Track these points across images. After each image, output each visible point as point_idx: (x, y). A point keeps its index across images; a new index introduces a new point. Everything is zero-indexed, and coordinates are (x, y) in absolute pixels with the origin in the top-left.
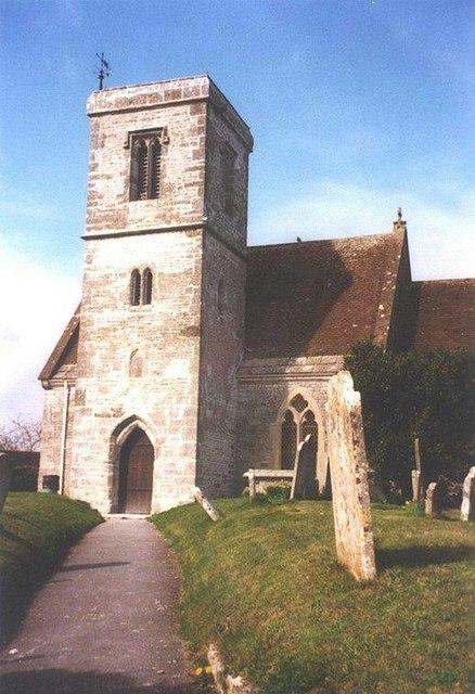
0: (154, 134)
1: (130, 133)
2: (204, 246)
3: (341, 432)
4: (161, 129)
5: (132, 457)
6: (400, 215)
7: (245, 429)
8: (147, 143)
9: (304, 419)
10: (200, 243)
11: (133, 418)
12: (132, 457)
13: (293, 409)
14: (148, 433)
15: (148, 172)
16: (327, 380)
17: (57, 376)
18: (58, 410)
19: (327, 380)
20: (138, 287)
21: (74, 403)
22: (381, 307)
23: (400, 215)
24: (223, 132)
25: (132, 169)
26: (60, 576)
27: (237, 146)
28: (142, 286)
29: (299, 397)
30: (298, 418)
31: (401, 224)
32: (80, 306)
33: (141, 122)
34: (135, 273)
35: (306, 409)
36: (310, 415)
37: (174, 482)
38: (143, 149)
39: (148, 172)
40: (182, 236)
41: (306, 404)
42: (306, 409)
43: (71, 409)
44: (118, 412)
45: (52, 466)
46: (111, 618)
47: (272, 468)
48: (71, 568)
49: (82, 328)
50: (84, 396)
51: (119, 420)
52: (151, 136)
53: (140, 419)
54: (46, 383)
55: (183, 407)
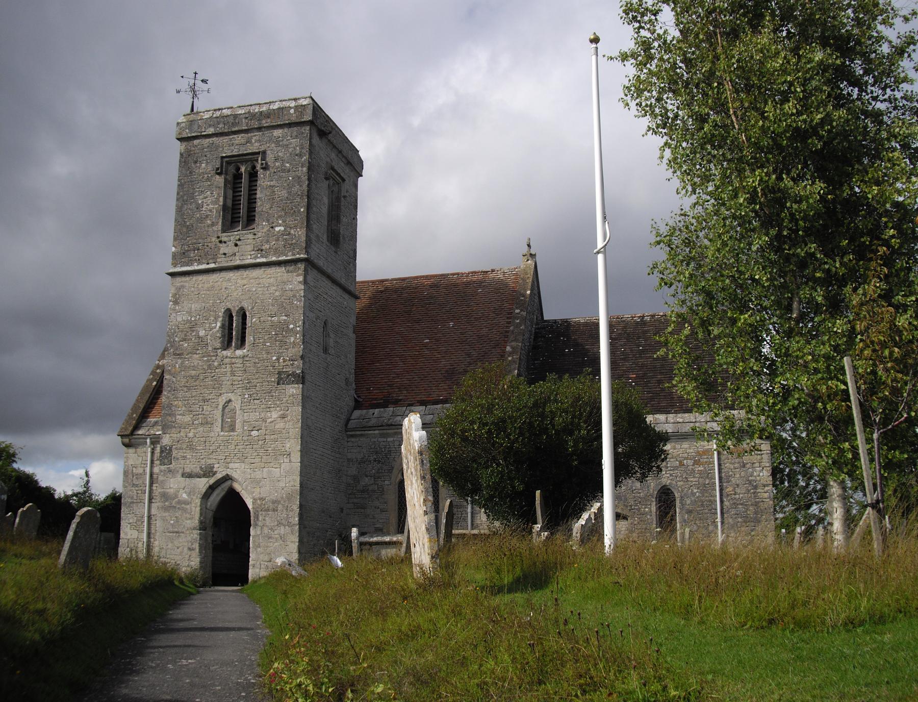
0: (250, 158)
1: (222, 157)
2: (305, 282)
3: (413, 470)
4: (258, 153)
5: (228, 520)
6: (529, 246)
7: (347, 499)
8: (243, 169)
10: (301, 278)
11: (227, 478)
12: (228, 520)
15: (243, 201)
17: (140, 432)
18: (140, 471)
19: (206, 496)
20: (231, 324)
21: (158, 462)
22: (508, 349)
23: (529, 246)
24: (325, 155)
25: (225, 198)
26: (164, 639)
27: (340, 166)
28: (235, 328)
32: (164, 351)
33: (233, 146)
34: (229, 314)
37: (273, 548)
38: (238, 176)
39: (243, 201)
40: (280, 271)
43: (156, 470)
44: (208, 472)
45: (135, 534)
46: (744, 15)
47: (388, 534)
48: (154, 647)
49: (167, 376)
51: (212, 481)
52: (246, 161)
54: (126, 440)
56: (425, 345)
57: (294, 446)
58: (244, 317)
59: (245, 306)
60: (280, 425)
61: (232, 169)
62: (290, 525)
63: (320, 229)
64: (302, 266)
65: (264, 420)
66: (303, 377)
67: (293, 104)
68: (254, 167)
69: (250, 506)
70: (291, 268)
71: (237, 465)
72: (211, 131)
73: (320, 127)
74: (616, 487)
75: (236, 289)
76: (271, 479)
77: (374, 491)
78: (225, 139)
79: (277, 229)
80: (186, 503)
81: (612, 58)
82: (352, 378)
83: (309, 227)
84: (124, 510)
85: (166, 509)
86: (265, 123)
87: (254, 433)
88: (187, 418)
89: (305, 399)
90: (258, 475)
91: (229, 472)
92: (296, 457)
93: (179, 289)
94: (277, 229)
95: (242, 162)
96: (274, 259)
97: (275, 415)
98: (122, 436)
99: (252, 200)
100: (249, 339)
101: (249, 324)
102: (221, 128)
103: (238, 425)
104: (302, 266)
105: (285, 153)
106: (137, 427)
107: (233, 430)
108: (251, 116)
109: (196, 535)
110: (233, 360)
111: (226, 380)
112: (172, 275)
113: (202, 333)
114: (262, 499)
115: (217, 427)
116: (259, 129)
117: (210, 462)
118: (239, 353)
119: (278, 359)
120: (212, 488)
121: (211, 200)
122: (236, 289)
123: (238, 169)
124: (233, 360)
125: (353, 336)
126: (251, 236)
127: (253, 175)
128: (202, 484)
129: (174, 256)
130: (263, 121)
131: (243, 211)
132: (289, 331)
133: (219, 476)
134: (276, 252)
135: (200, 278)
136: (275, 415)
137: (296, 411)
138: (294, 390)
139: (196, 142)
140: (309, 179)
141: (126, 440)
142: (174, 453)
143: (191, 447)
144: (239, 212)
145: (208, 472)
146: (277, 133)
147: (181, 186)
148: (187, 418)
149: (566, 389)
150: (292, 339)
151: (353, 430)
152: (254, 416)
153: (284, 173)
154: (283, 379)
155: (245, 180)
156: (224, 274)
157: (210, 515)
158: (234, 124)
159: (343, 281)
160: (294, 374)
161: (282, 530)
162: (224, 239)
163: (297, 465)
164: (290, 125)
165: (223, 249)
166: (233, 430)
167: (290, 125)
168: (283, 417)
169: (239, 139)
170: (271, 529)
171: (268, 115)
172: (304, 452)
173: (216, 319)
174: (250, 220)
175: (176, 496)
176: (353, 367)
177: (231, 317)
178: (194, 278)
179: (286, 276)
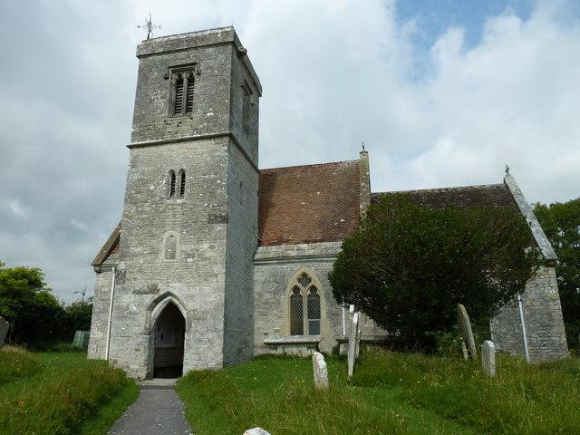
0: (190, 67)
2: (229, 151)
9: (309, 293)
13: (300, 285)
14: (181, 308)
16: (151, 308)
18: (107, 290)
19: (151, 308)
20: (173, 185)
25: (171, 95)
28: (177, 183)
29: (304, 275)
30: (305, 292)
31: (364, 153)
33: (182, 59)
35: (311, 284)
36: (313, 289)
41: (310, 280)
42: (311, 284)
44: (154, 290)
50: (430, 347)
51: (156, 297)
53: (175, 296)
54: (98, 268)
55: (132, 344)
56: (303, 206)
57: (220, 269)
58: (183, 176)
59: (184, 168)
61: (175, 77)
62: (216, 330)
63: (238, 117)
64: (227, 139)
66: (227, 218)
67: (220, 31)
68: (191, 75)
69: (185, 317)
70: (218, 141)
71: (176, 284)
73: (232, 45)
75: (176, 156)
76: (201, 298)
77: (273, 303)
78: (172, 56)
80: (135, 313)
81: (507, 171)
82: (256, 226)
83: (231, 113)
84: (94, 317)
85: (120, 318)
87: (190, 260)
88: (139, 250)
89: (229, 234)
90: (193, 291)
92: (222, 278)
93: (135, 157)
95: (183, 71)
97: (206, 246)
98: (95, 266)
99: (190, 98)
100: (187, 191)
101: (187, 180)
103: (178, 254)
104: (227, 139)
105: (214, 64)
106: (104, 260)
108: (189, 40)
109: (144, 339)
111: (169, 221)
112: (130, 147)
113: (152, 187)
114: (194, 310)
115: (162, 256)
116: (196, 48)
117: (155, 282)
118: (179, 201)
120: (156, 302)
122: (176, 156)
123: (180, 76)
125: (257, 197)
126: (189, 120)
127: (191, 81)
128: (149, 299)
129: (133, 134)
130: (196, 43)
131: (184, 103)
133: (162, 293)
136: (206, 246)
137: (222, 245)
139: (151, 58)
140: (232, 80)
141: (98, 268)
142: (127, 276)
143: (140, 271)
144: (181, 105)
145: (154, 290)
146: (210, 50)
147: (139, 87)
148: (139, 250)
151: (258, 260)
153: (199, 80)
154: (215, 219)
155: (185, 81)
156: (169, 146)
157: (153, 322)
159: (249, 154)
160: (221, 217)
161: (210, 335)
162: (170, 122)
163: (222, 284)
164: (217, 45)
167: (217, 45)
169: (182, 54)
170: (202, 334)
171: (202, 39)
172: (228, 274)
174: (189, 108)
175: (128, 308)
176: (257, 218)
177: (174, 176)
178: (147, 149)
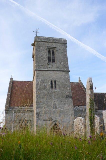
33: (50, 45)
52: (52, 49)
58: (55, 82)
60: (68, 108)
65: (64, 107)
72: (44, 41)
74: (10, 106)
79: (62, 64)
86: (56, 42)
91: (56, 119)
94: (62, 64)
95: (51, 49)
96: (62, 70)
97: (67, 105)
102: (46, 41)
107: (56, 109)
110: (55, 92)
116: (55, 43)
119: (66, 92)
121: (45, 55)
124: (55, 92)
132: (68, 86)
134: (62, 69)
135: (44, 72)
138: (71, 100)
139: (40, 42)
141: (7, 112)
149: (38, 111)
150: (69, 88)
152: (61, 106)
154: (68, 97)
158: (49, 40)
162: (49, 64)
165: (49, 66)
166: (56, 109)
168: (69, 106)
169: (50, 44)
171: (57, 40)
173: (49, 82)
179: (65, 74)
